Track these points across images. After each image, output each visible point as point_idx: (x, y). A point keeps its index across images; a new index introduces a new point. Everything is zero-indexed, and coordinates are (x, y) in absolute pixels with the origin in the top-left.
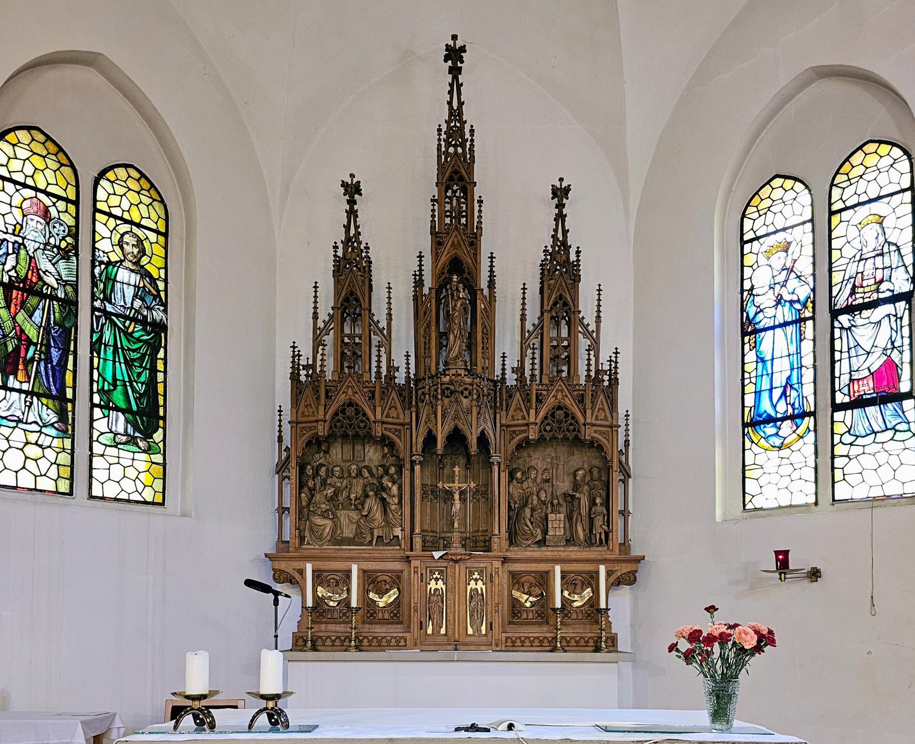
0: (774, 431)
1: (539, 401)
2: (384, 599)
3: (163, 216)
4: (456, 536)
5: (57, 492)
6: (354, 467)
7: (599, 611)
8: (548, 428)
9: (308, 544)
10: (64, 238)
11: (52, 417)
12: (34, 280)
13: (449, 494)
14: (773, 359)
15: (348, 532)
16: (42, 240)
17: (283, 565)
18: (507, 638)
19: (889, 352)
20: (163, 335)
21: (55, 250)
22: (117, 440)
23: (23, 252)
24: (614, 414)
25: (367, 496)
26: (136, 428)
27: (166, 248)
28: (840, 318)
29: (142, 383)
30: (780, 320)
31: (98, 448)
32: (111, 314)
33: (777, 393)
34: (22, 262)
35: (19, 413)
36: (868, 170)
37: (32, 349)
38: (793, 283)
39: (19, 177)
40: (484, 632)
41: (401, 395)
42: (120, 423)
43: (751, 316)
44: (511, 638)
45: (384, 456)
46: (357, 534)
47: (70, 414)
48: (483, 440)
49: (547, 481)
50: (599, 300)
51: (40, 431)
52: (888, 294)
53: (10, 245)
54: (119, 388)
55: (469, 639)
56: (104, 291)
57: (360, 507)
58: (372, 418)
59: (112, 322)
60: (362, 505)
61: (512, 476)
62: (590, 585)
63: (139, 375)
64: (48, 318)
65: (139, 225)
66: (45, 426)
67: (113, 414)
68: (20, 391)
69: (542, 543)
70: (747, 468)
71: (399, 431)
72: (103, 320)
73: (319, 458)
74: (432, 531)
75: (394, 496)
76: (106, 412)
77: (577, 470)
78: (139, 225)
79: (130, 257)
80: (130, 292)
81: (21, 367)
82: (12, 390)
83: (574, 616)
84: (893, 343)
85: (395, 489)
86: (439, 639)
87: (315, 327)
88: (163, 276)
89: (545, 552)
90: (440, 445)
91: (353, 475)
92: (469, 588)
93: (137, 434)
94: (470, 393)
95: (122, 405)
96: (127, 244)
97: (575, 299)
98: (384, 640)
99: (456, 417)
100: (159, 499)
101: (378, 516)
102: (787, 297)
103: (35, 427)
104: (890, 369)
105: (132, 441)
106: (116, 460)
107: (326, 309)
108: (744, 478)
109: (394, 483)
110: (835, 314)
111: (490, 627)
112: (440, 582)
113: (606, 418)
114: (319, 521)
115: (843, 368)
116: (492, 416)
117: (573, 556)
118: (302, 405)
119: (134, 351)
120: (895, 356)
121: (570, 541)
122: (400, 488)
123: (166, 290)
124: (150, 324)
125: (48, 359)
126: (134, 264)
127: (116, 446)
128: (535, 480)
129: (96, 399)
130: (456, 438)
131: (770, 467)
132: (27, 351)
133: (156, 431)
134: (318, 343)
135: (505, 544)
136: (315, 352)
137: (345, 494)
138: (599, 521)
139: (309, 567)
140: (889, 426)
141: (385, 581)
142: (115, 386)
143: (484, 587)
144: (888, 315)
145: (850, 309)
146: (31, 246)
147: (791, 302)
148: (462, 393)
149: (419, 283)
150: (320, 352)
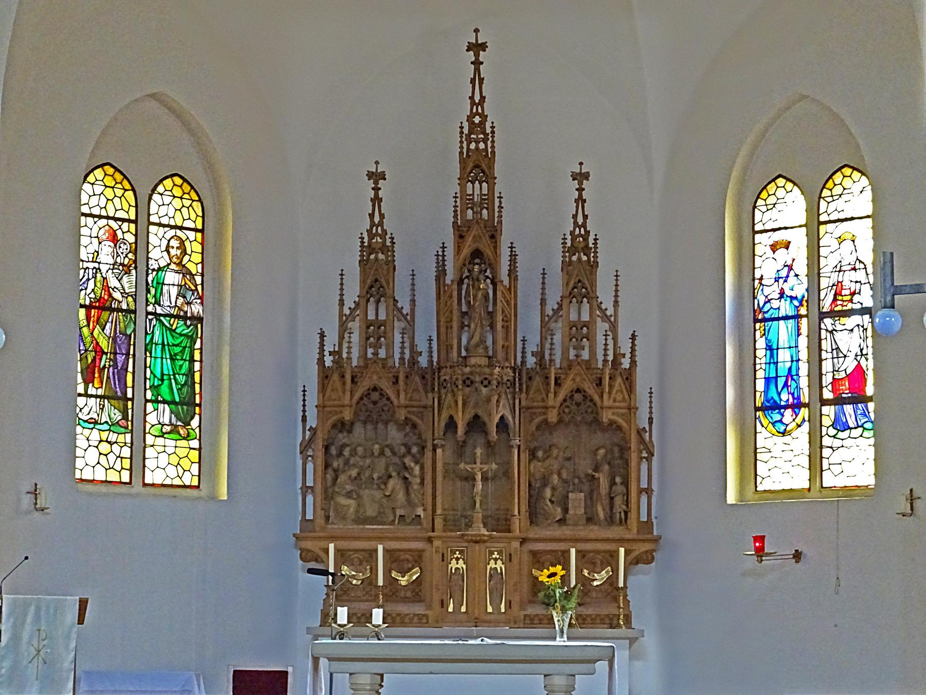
0: (778, 417)
1: (557, 383)
2: (406, 578)
3: (200, 214)
4: (478, 516)
5: (121, 482)
6: (377, 446)
7: (618, 589)
8: (567, 410)
9: (333, 523)
10: (126, 256)
11: (117, 416)
12: (106, 297)
13: (469, 478)
14: (778, 349)
15: (371, 512)
16: (112, 262)
17: (308, 545)
18: (525, 616)
19: (859, 358)
20: (199, 326)
21: (121, 268)
22: (164, 430)
23: (99, 275)
24: (632, 396)
25: (390, 477)
26: (178, 418)
27: (202, 244)
28: (825, 320)
29: (183, 375)
30: (782, 313)
31: (150, 440)
32: (161, 315)
33: (781, 382)
34: (98, 284)
35: (95, 416)
36: (846, 191)
37: (104, 357)
38: (792, 279)
39: (96, 211)
40: (503, 611)
41: (424, 378)
42: (167, 414)
43: (761, 305)
44: (529, 616)
45: (406, 435)
46: (380, 513)
47: (130, 411)
48: (503, 425)
49: (569, 459)
50: (617, 285)
51: (110, 430)
52: (858, 306)
53: (91, 271)
54: (166, 382)
55: (489, 617)
56: (155, 296)
57: (383, 487)
58: (396, 402)
59: (161, 321)
60: (385, 484)
61: (533, 455)
62: (609, 564)
63: (181, 366)
64: (115, 329)
65: (181, 228)
66: (113, 425)
67: (161, 406)
68: (96, 396)
69: (562, 521)
70: (758, 451)
71: (421, 413)
72: (154, 322)
73: (342, 438)
74: (454, 510)
75: (415, 476)
76: (155, 405)
77: (597, 450)
78: (181, 228)
79: (175, 260)
80: (174, 291)
81: (96, 375)
82: (91, 396)
83: (594, 594)
84: (861, 350)
85: (417, 469)
86: (460, 617)
87: (341, 314)
88: (200, 271)
89: (566, 531)
90: (461, 431)
91: (376, 454)
92: (489, 567)
93: (179, 423)
94: (489, 383)
95: (168, 398)
96: (173, 247)
97: (593, 284)
98: (407, 617)
99: (476, 405)
100: (195, 483)
101: (401, 496)
102: (788, 292)
103: (106, 427)
104: (858, 375)
105: (175, 430)
106: (162, 449)
107: (352, 294)
108: (756, 460)
109: (416, 463)
110: (822, 316)
111: (509, 605)
112: (461, 561)
113: (624, 400)
114: (343, 501)
115: (827, 366)
116: (511, 402)
117: (592, 536)
118: (329, 389)
119: (176, 346)
120: (863, 363)
121: (590, 519)
122: (422, 468)
123: (202, 284)
124: (190, 318)
125: (115, 366)
126: (178, 264)
127: (162, 436)
128: (556, 458)
129: (149, 395)
130: (476, 424)
131: (776, 451)
132: (101, 359)
133: (192, 418)
134: (343, 329)
135: (526, 523)
136: (341, 338)
137: (367, 473)
138: (618, 501)
139: (332, 547)
140: (860, 424)
141: (407, 560)
142: (162, 380)
143: (503, 567)
144: (858, 325)
145: (833, 314)
146: (104, 268)
147: (792, 298)
148: (482, 383)
149: (441, 273)
150: (347, 339)
